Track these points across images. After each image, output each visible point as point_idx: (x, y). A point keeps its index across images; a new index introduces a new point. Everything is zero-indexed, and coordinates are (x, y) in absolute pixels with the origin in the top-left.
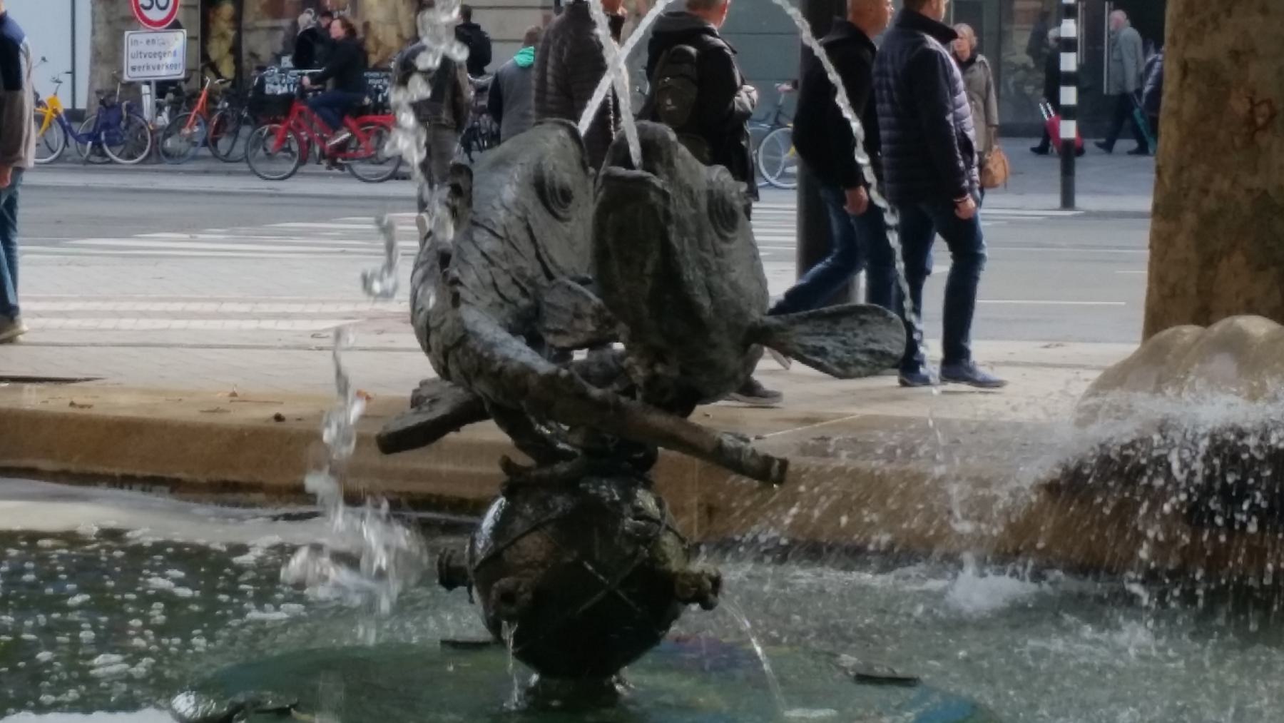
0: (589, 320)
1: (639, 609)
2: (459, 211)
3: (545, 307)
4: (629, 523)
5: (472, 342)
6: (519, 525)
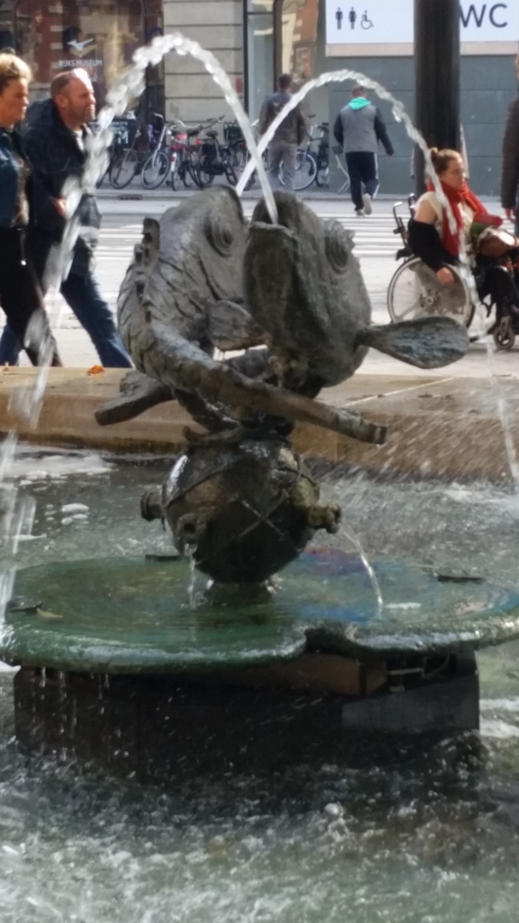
0: (243, 329)
1: (283, 534)
2: (150, 253)
3: (212, 321)
4: (274, 473)
5: (160, 347)
6: (196, 475)
